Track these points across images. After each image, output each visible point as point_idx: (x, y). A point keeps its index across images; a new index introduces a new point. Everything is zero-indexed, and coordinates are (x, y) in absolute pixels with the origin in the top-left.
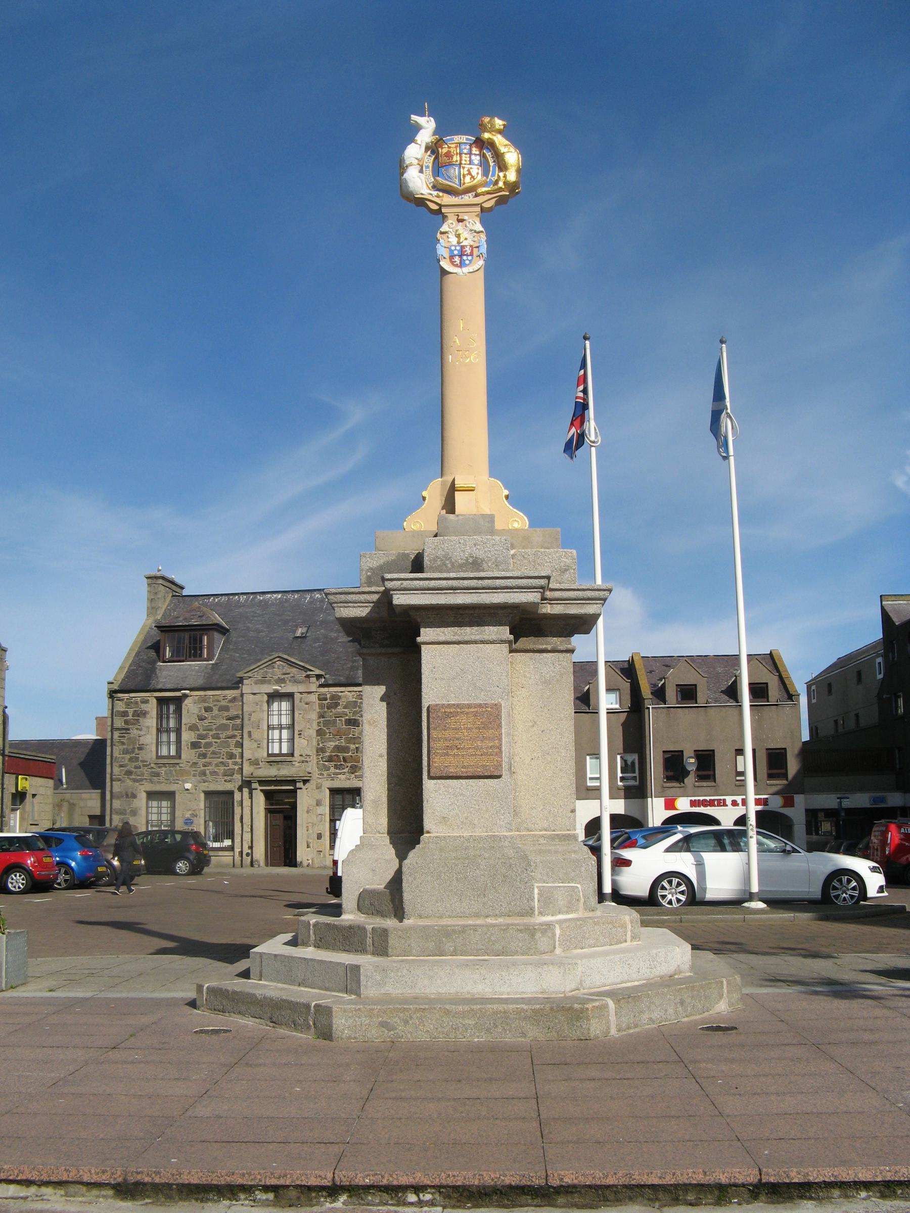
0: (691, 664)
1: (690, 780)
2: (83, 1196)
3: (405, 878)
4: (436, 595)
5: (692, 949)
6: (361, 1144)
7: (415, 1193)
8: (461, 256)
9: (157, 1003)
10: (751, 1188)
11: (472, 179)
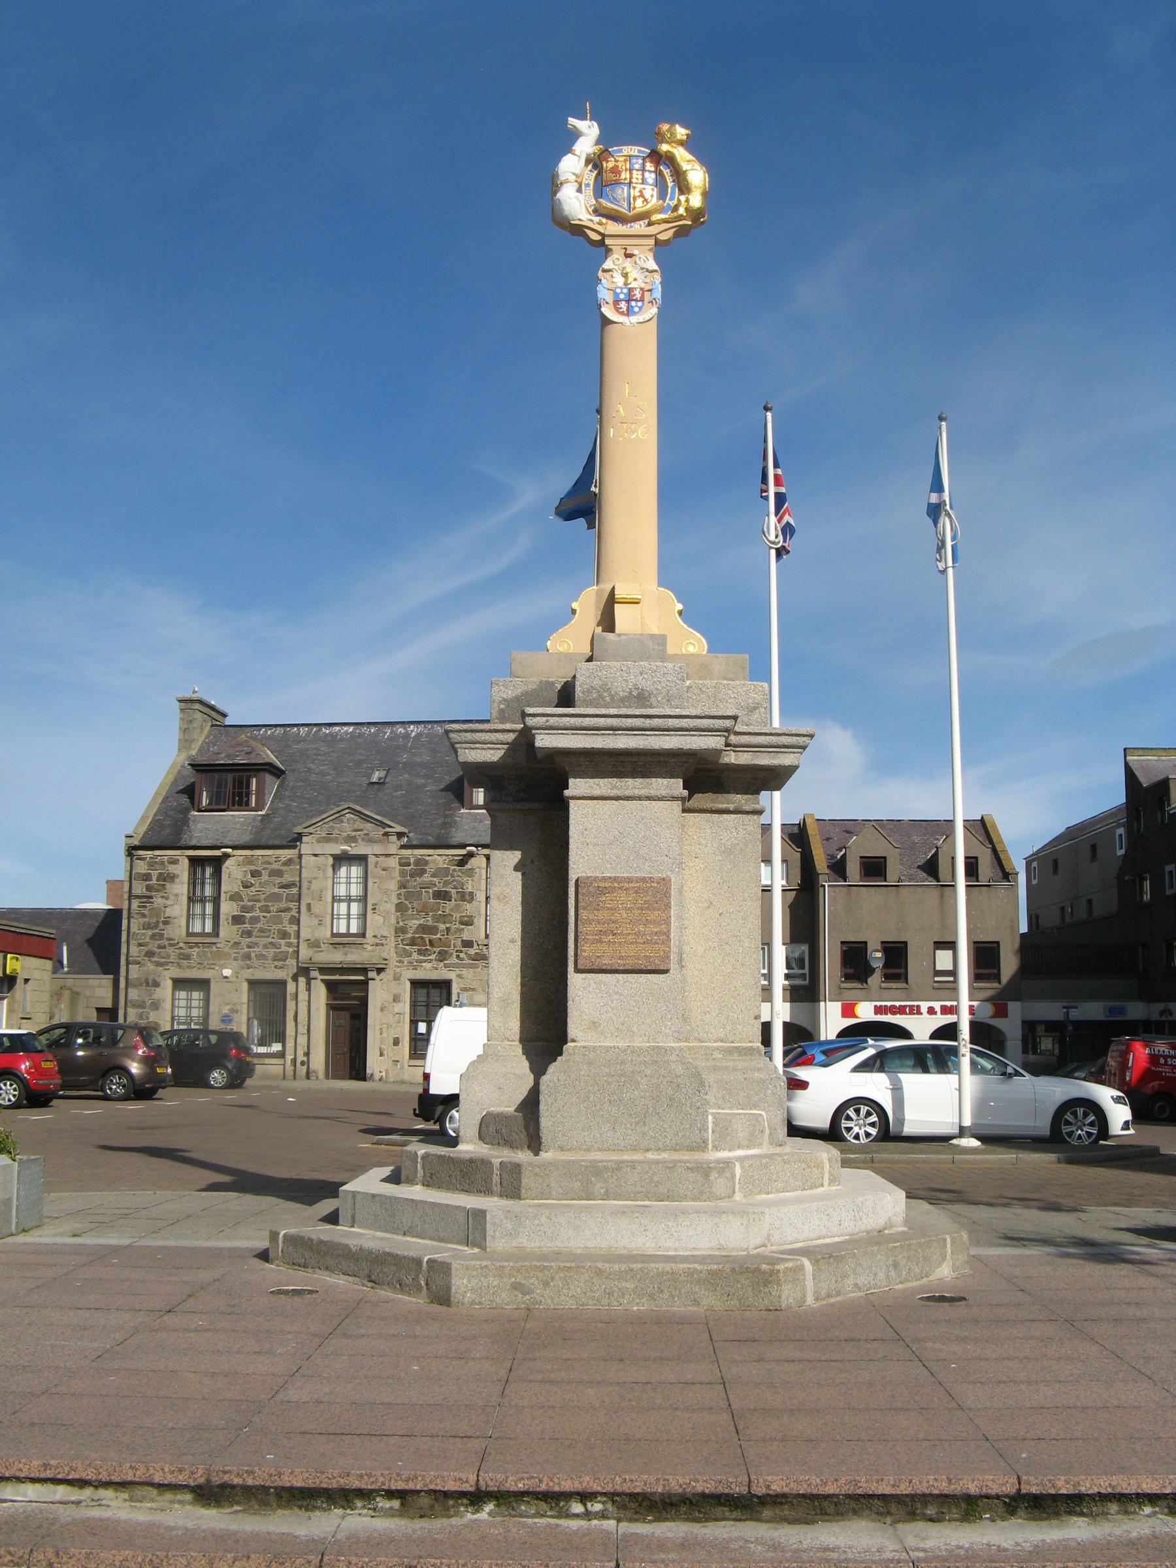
0: (880, 830)
1: (875, 980)
2: (153, 1501)
3: (542, 1099)
4: (591, 736)
5: (907, 1197)
6: (507, 1438)
7: (581, 1502)
8: (628, 301)
9: (217, 1255)
10: (1007, 1500)
11: (645, 203)
